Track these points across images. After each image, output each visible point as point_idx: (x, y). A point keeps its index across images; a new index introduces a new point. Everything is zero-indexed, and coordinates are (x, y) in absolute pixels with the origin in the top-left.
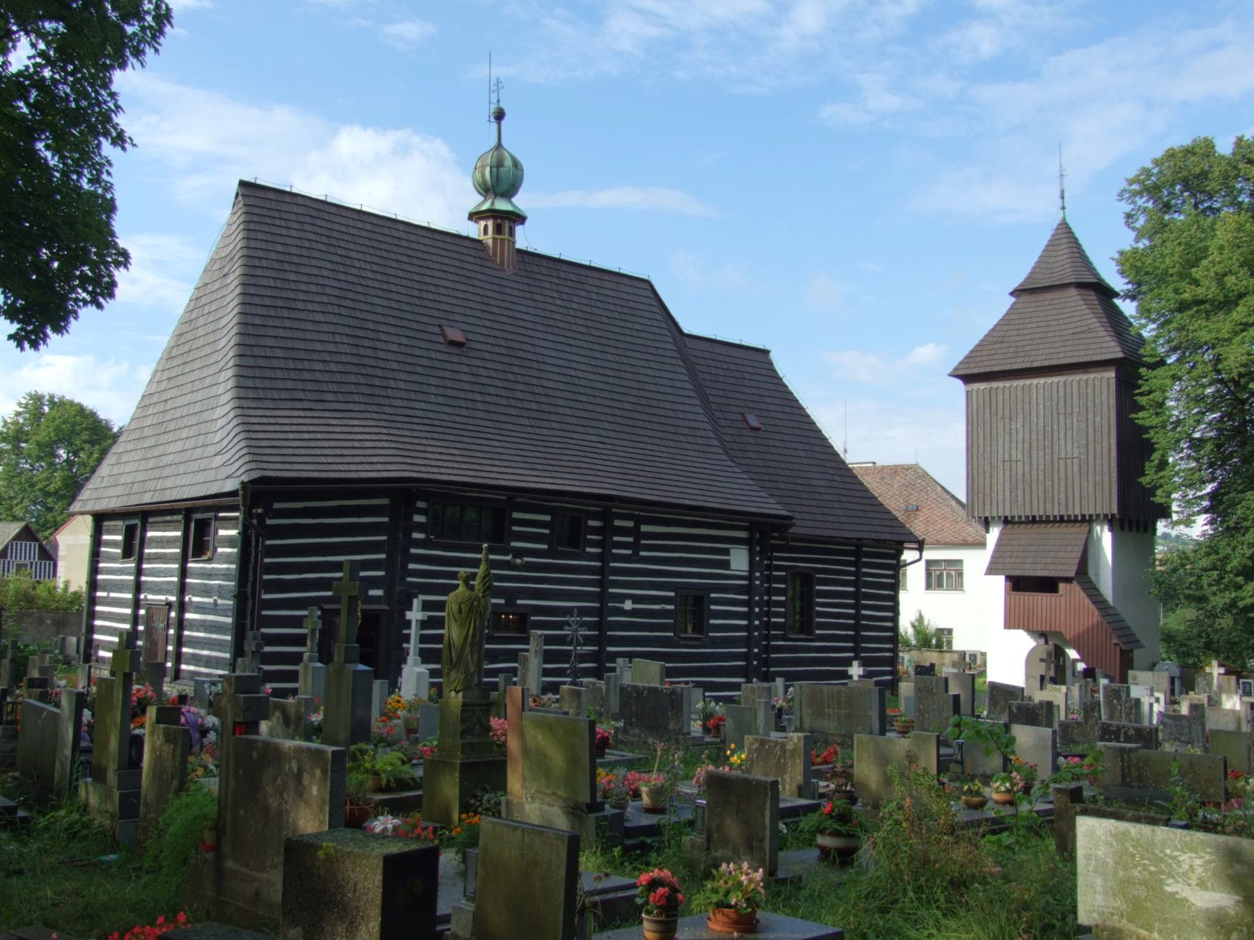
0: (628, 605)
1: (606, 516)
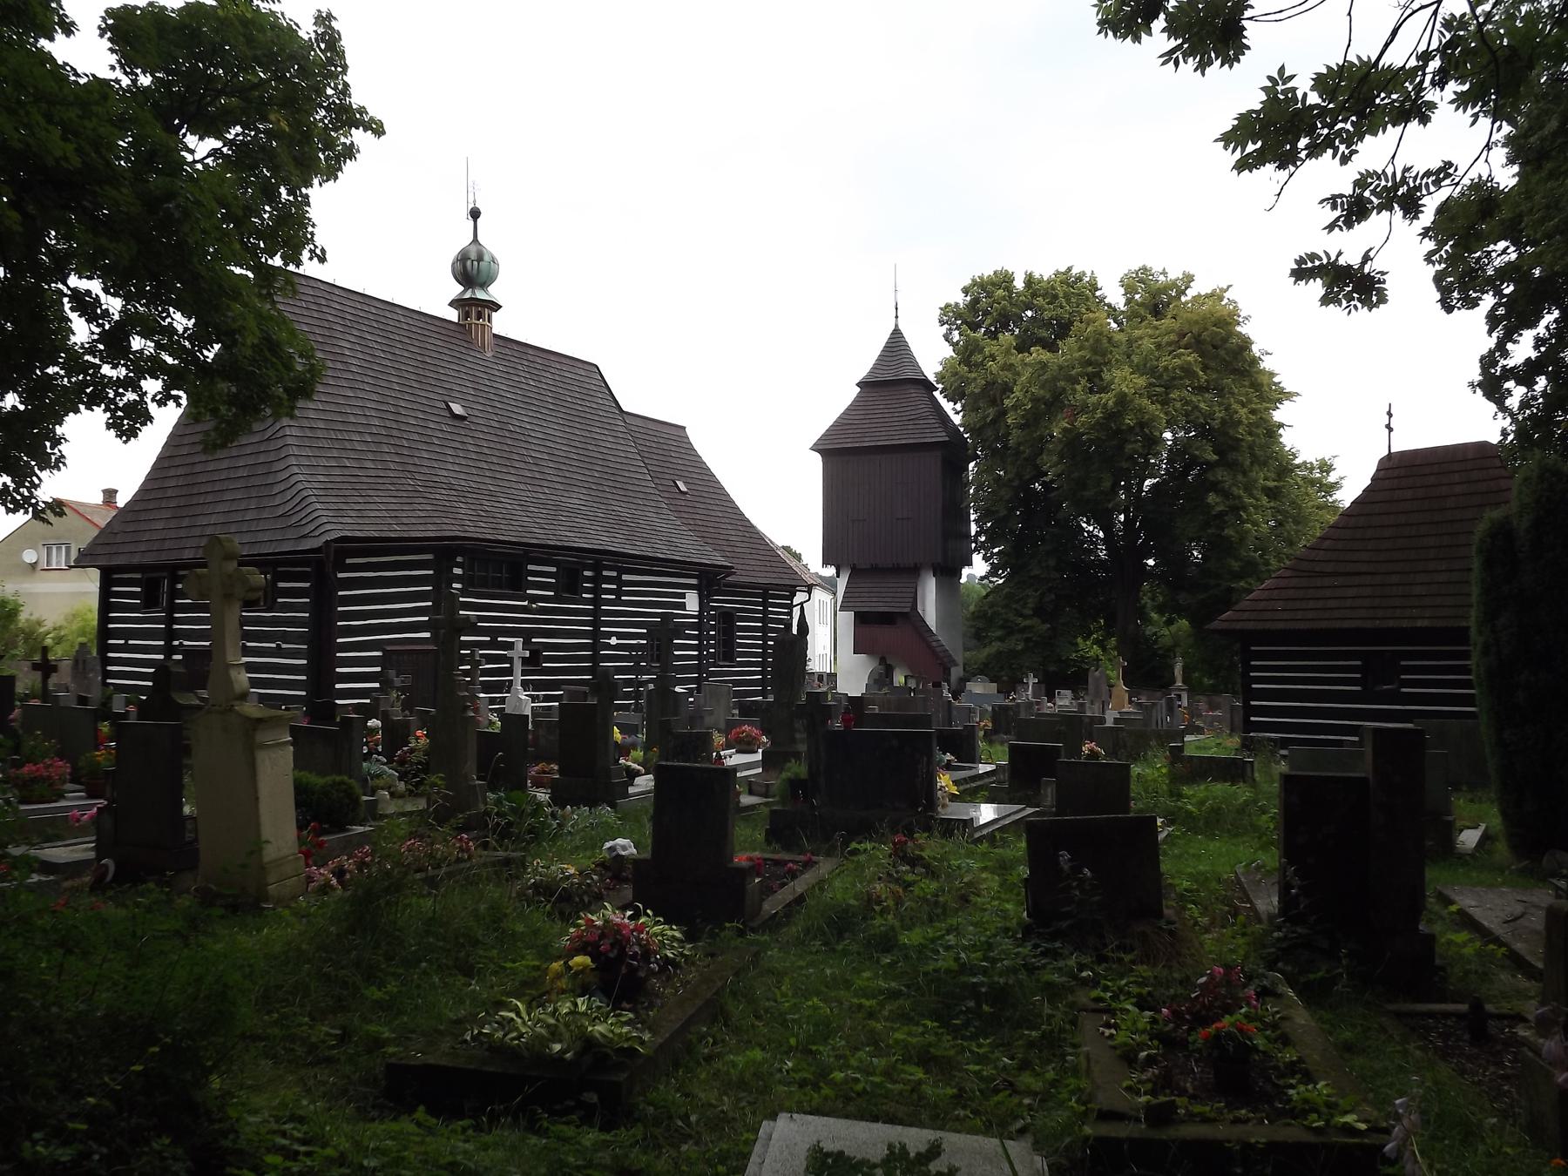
0: (614, 641)
1: (597, 568)
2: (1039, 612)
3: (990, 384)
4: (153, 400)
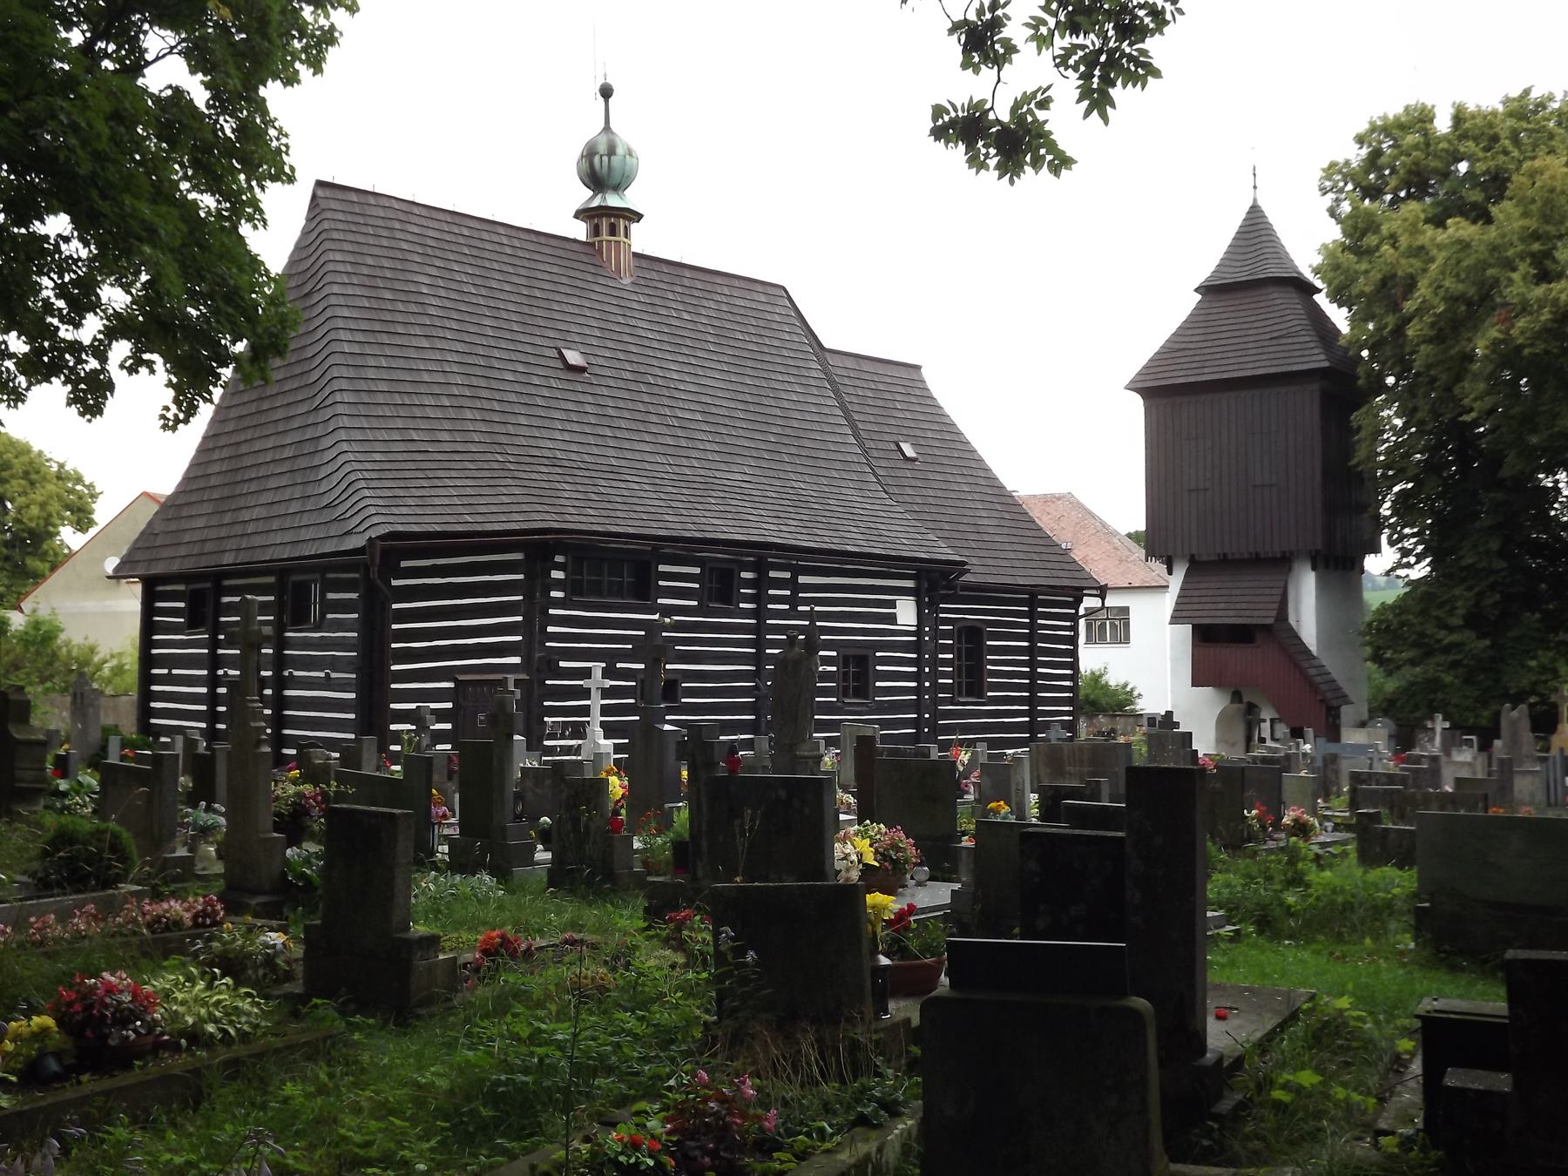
1: (761, 567)
2: (1474, 621)
3: (1386, 282)
4: (122, 366)
